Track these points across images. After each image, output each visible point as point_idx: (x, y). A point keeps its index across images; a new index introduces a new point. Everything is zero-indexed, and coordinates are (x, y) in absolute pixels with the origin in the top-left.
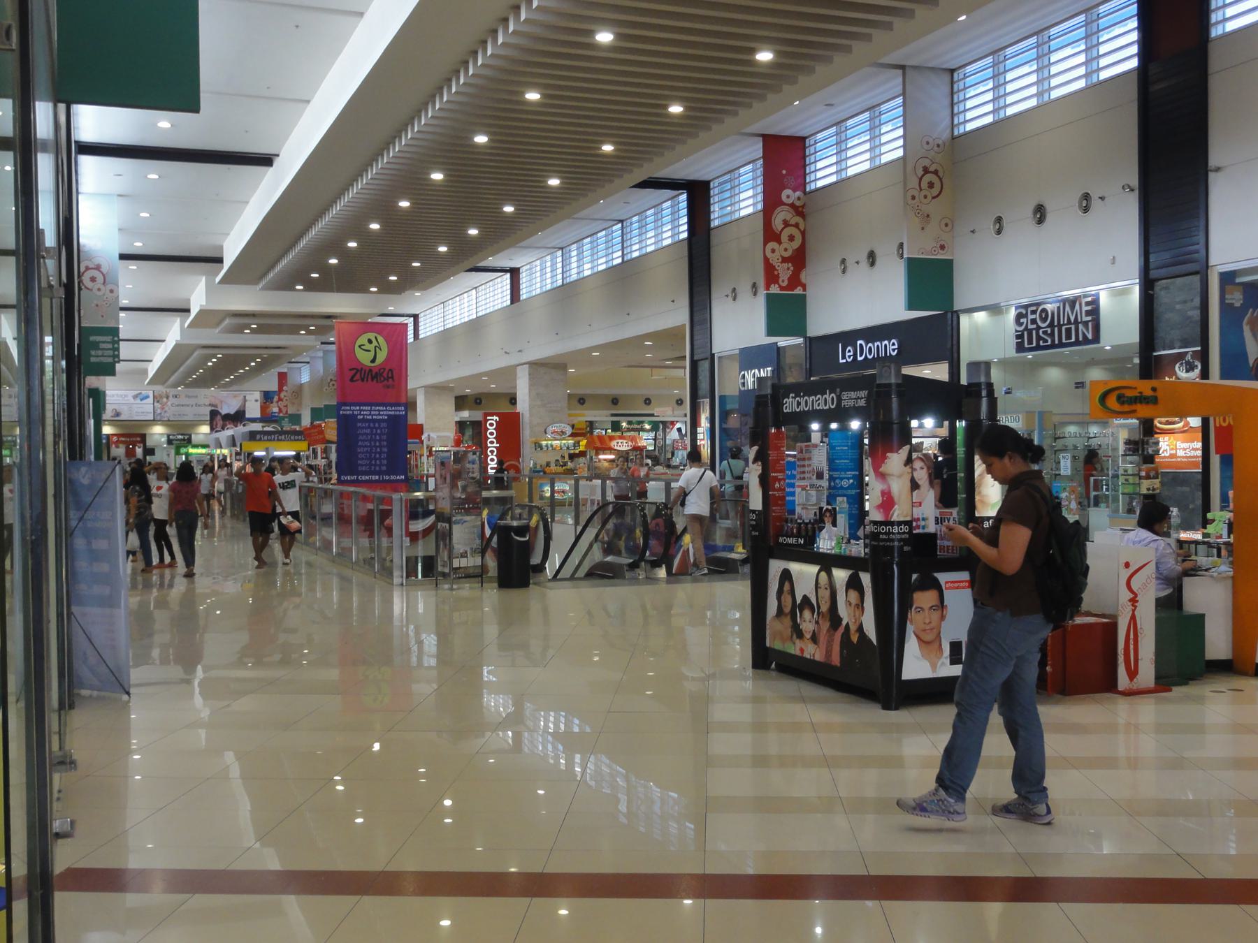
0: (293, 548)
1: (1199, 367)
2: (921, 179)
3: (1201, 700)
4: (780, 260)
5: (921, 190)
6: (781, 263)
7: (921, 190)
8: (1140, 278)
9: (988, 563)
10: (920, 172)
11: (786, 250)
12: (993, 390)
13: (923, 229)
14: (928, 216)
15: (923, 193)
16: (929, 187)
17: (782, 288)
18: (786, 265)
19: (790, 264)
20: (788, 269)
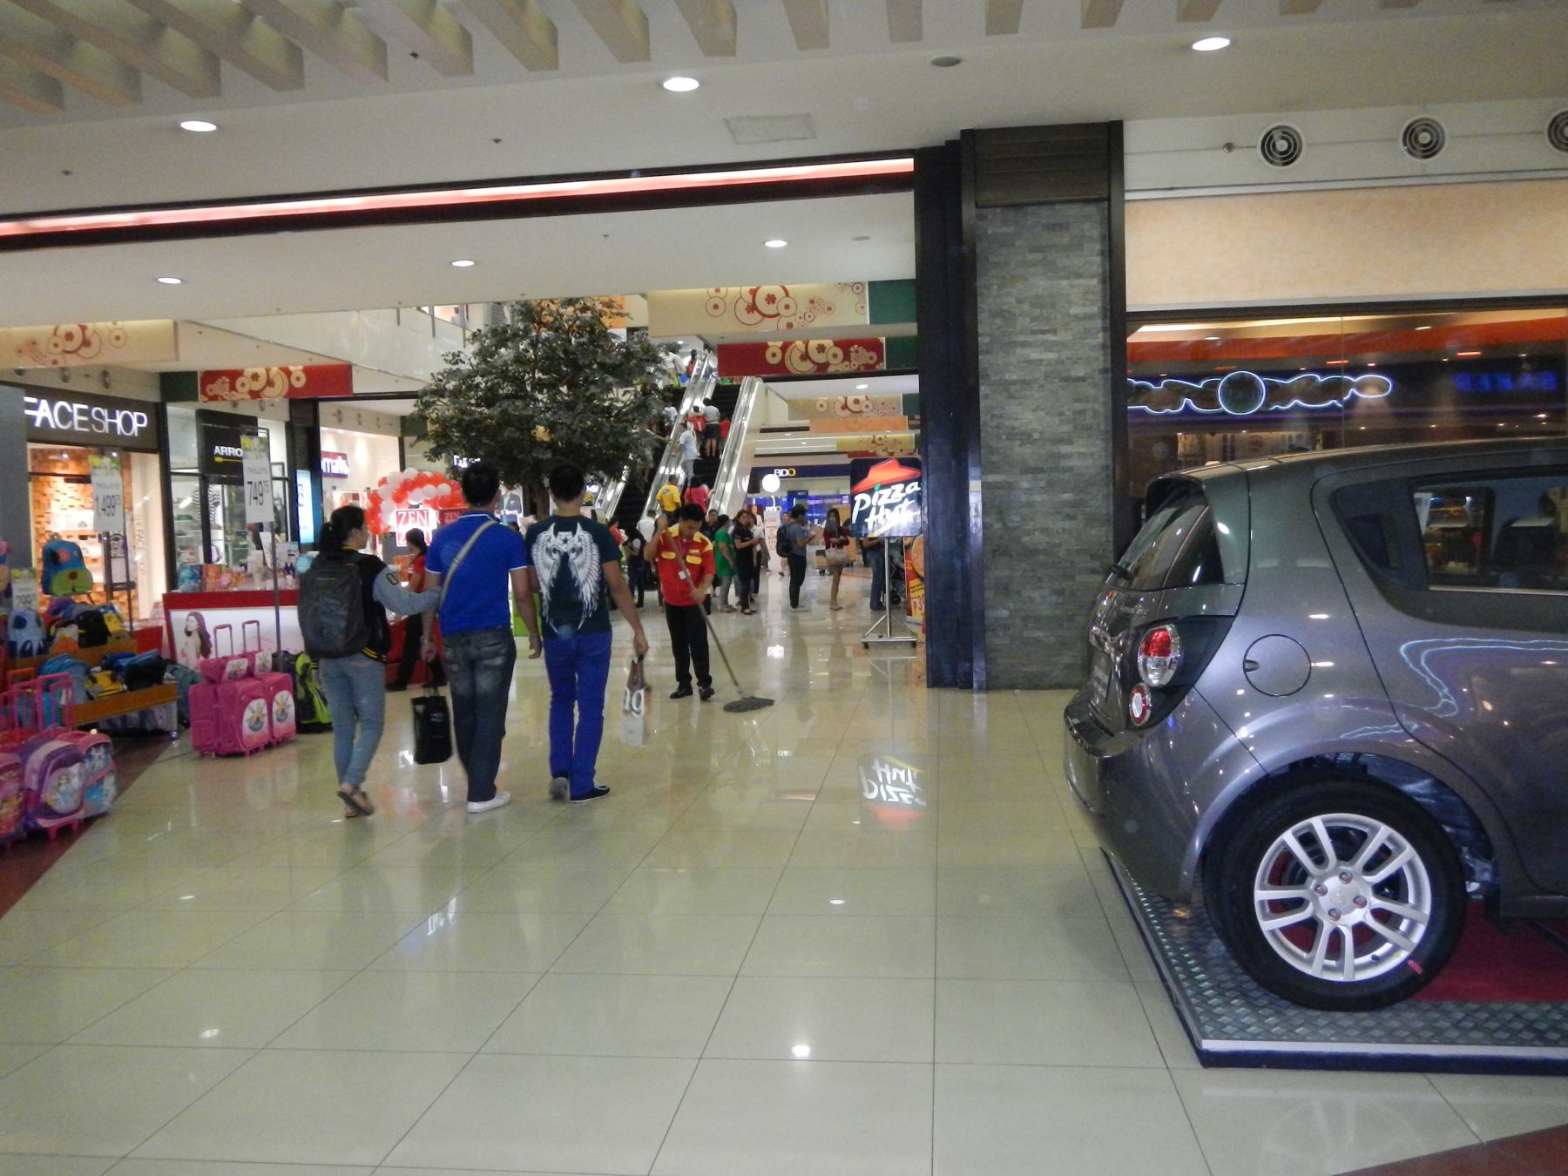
0: (842, 577)
1: (246, 725)
2: (765, 316)
3: (766, 596)
4: (847, 363)
5: (777, 315)
6: (850, 361)
7: (777, 315)
8: (1124, 201)
9: (1376, 592)
10: (756, 316)
11: (835, 356)
12: (600, 719)
13: (830, 309)
14: (812, 302)
15: (783, 311)
16: (773, 302)
17: (880, 359)
18: (853, 355)
19: (852, 349)
20: (857, 351)
